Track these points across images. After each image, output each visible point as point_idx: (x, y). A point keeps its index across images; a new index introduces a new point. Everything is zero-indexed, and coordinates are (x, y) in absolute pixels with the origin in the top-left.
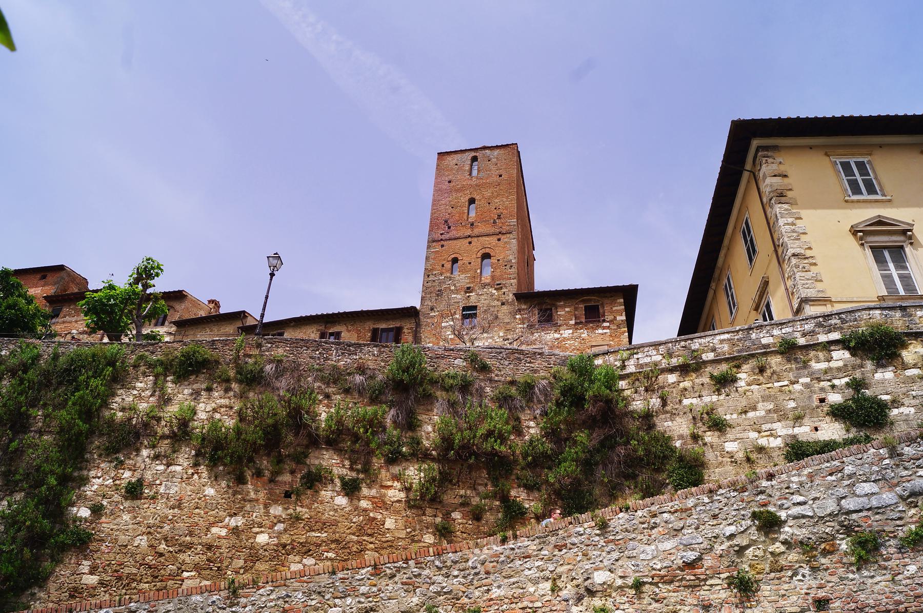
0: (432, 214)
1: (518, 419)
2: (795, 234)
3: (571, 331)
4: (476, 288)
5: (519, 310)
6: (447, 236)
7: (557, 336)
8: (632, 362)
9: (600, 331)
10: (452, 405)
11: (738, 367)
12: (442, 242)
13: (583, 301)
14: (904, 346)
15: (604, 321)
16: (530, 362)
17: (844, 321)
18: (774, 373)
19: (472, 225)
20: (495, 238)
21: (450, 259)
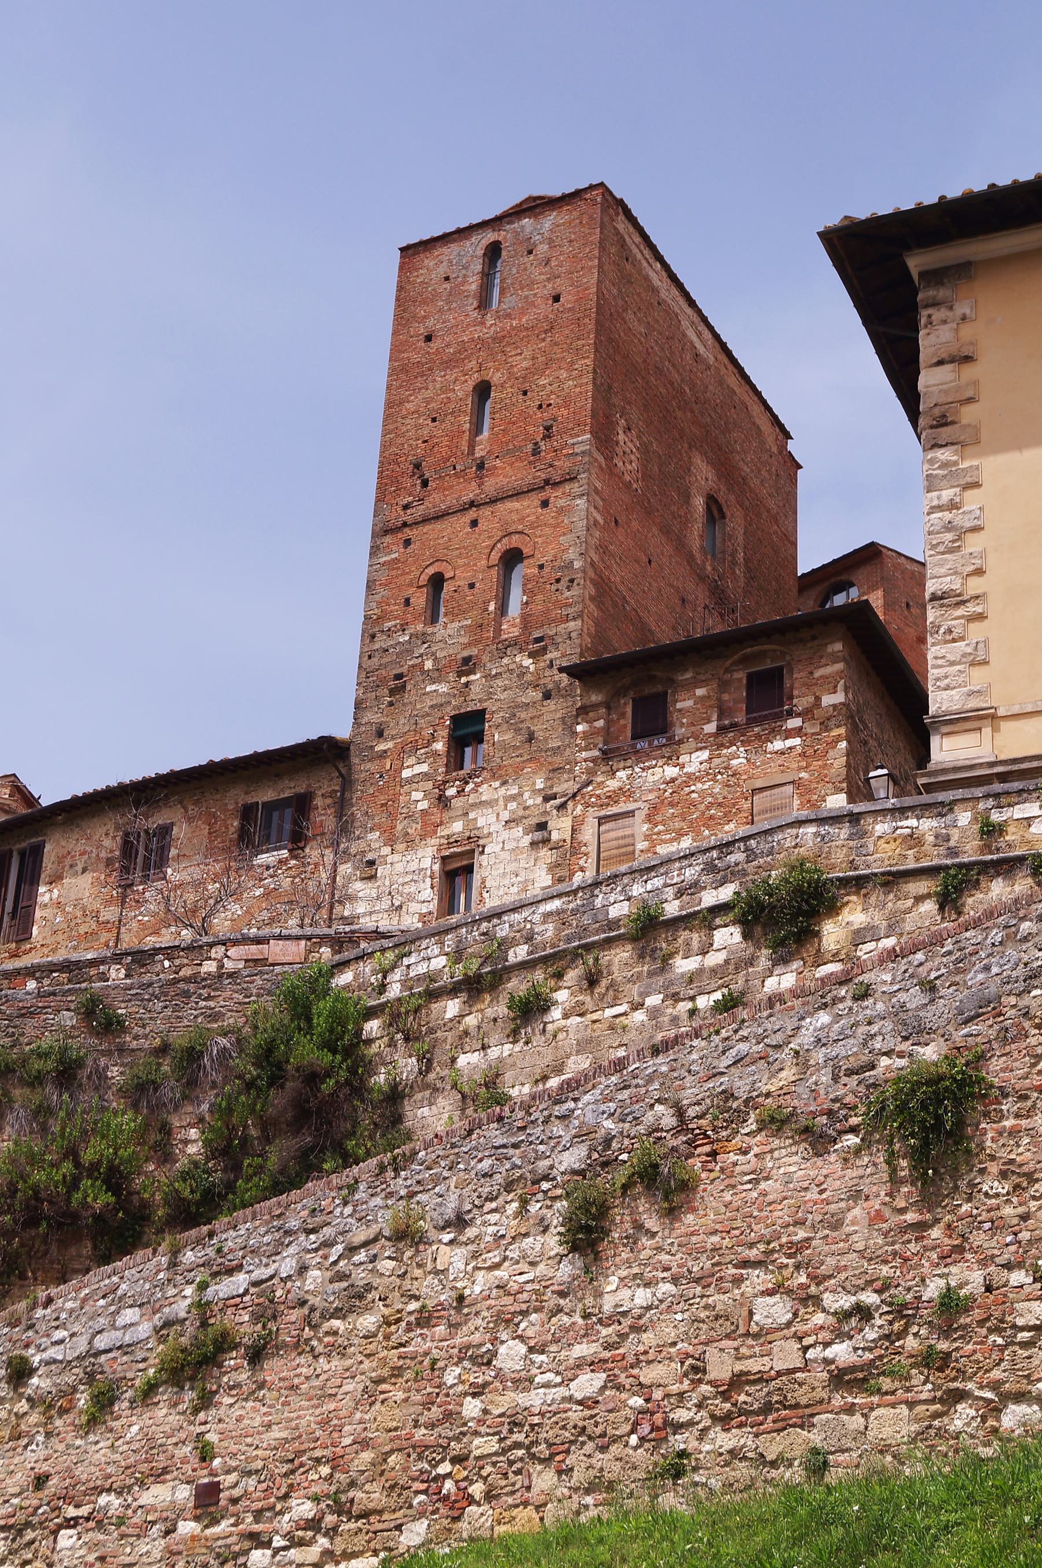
0: (384, 447)
1: (166, 1130)
2: (949, 536)
3: (705, 755)
4: (485, 658)
5: (583, 712)
6: (418, 511)
7: (671, 771)
8: (397, 975)
9: (778, 745)
10: (42, 1112)
11: (559, 976)
12: (408, 532)
13: (745, 661)
14: (833, 909)
15: (790, 714)
16: (209, 998)
17: (751, 855)
18: (612, 985)
19: (481, 466)
20: (535, 499)
21: (424, 579)
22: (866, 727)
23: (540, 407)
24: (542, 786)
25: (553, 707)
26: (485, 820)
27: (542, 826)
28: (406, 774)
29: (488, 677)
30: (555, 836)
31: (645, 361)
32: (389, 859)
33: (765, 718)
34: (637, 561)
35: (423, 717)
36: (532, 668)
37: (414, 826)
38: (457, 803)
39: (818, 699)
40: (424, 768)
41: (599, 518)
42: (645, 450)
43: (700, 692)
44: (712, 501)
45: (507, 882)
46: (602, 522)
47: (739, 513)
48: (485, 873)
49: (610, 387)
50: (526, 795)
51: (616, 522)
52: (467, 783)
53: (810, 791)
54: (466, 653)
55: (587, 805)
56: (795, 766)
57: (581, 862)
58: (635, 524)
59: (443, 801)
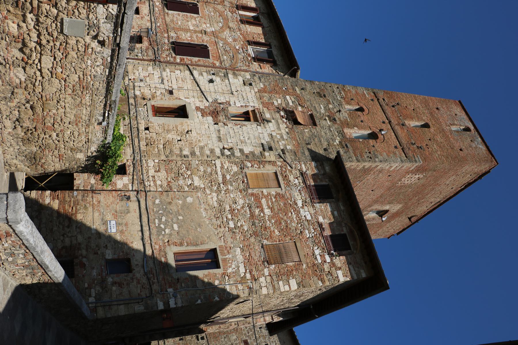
4: (336, 126)
6: (385, 107)
12: (376, 100)
15: (331, 255)
21: (362, 105)
24: (288, 148)
26: (272, 126)
27: (271, 149)
28: (288, 97)
30: (267, 154)
35: (311, 104)
36: (335, 144)
37: (267, 100)
38: (278, 115)
39: (340, 269)
40: (291, 104)
41: (393, 168)
42: (410, 186)
44: (386, 212)
45: (245, 135)
48: (249, 126)
49: (435, 171)
51: (389, 176)
52: (286, 119)
54: (337, 119)
55: (281, 167)
57: (256, 166)
59: (278, 109)
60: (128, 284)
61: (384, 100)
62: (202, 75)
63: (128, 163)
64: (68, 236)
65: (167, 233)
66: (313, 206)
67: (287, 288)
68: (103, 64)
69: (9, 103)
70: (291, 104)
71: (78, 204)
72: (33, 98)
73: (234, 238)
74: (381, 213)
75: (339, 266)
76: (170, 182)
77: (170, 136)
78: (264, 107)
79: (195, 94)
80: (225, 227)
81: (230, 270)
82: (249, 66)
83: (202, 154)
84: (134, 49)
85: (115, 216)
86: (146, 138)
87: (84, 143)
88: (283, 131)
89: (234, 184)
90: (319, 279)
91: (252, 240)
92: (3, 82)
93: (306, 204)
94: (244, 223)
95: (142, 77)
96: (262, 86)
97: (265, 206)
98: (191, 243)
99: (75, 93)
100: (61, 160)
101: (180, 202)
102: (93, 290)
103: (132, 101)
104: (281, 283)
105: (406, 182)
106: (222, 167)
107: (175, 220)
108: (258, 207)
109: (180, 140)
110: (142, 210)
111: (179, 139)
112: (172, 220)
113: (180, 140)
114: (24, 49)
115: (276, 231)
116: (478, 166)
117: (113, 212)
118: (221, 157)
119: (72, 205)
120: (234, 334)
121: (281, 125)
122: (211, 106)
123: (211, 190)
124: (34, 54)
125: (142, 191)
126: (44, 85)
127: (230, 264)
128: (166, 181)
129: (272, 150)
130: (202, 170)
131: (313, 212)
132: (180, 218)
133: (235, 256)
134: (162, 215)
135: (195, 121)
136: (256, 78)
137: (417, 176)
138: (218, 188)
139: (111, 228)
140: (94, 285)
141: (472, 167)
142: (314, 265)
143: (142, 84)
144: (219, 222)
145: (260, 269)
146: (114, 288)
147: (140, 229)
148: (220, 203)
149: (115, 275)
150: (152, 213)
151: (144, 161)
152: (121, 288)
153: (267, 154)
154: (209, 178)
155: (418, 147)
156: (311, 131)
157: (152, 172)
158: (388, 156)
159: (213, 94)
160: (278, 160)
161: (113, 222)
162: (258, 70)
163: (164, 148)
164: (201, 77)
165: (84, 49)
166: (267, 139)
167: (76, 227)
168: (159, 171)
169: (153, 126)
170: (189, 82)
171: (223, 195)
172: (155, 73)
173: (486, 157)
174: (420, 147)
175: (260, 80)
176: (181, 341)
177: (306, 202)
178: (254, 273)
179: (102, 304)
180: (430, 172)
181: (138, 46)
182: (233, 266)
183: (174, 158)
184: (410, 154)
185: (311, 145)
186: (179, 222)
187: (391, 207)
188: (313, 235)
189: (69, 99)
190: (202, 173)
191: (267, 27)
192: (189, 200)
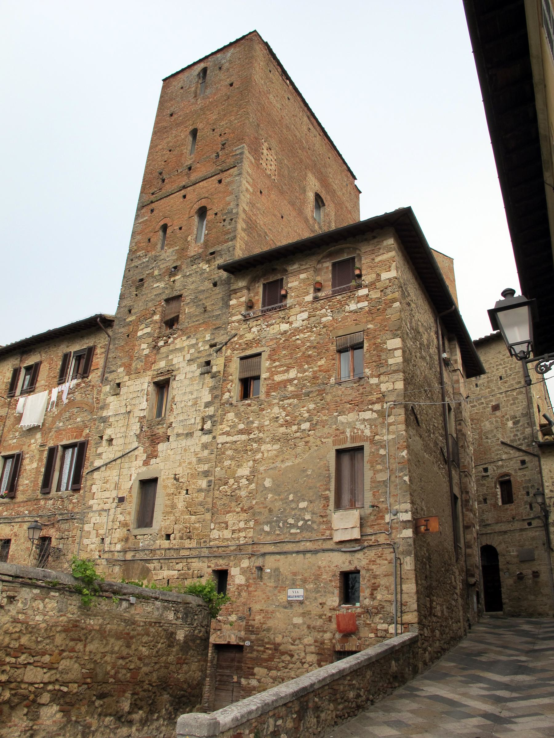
4: (184, 267)
6: (159, 195)
7: (284, 327)
12: (153, 205)
13: (330, 255)
15: (359, 287)
22: (409, 295)
23: (221, 135)
24: (209, 338)
25: (217, 291)
26: (177, 360)
27: (208, 363)
28: (140, 333)
29: (184, 276)
30: (214, 369)
31: (280, 121)
32: (128, 383)
33: (344, 290)
34: (275, 216)
35: (151, 301)
36: (208, 270)
37: (141, 364)
38: (163, 350)
39: (378, 275)
40: (148, 330)
41: (249, 187)
42: (279, 162)
43: (302, 276)
44: (318, 197)
45: (186, 398)
46: (251, 190)
47: (332, 205)
48: (175, 392)
49: (258, 125)
50: (200, 344)
51: (261, 192)
52: (169, 338)
53: (374, 338)
54: (175, 265)
55: (234, 349)
56: (365, 320)
57: (229, 386)
58: (273, 196)
59: (156, 348)
60: (375, 577)
61: (153, 194)
62: (100, 454)
63: (213, 566)
64: (305, 658)
65: (310, 518)
66: (290, 308)
67: (399, 353)
68: (43, 600)
69: (93, 729)
70: (148, 330)
71: (263, 640)
72: (87, 696)
73: (324, 424)
74: (319, 201)
75: (374, 276)
76: (242, 509)
77: (181, 506)
78: (151, 368)
79: (126, 465)
80: (309, 436)
81: (367, 432)
82: (93, 386)
83: (207, 461)
84: (58, 549)
85: (283, 589)
86: (181, 538)
87: (160, 629)
88: (186, 343)
89: (251, 419)
90: (391, 307)
91: (329, 398)
92: (59, 735)
93: (287, 318)
94: (305, 408)
95: (98, 540)
96: (122, 369)
97: (285, 377)
98: (326, 485)
99: (83, 638)
100: (186, 661)
101: (270, 496)
102: (379, 627)
103: (129, 556)
104: (391, 361)
105: (273, 167)
106: (228, 434)
107: (293, 505)
108: (285, 387)
109: (187, 490)
110: (276, 551)
111: (185, 492)
112: (293, 509)
113: (187, 490)
114: (13, 704)
115: (319, 363)
116: (256, 60)
117: (276, 592)
118: (214, 434)
119: (262, 649)
120: (482, 425)
121: (177, 347)
122: (143, 444)
123: (258, 450)
124: (20, 691)
125: (250, 550)
126: (67, 681)
127: (360, 432)
128: (240, 514)
129: (210, 361)
130: (229, 461)
131: (297, 309)
132: (291, 497)
133: (348, 423)
134: (285, 522)
135: (162, 468)
136: (111, 377)
137: (265, 151)
138: (256, 442)
139: (298, 596)
140: (373, 625)
141: (257, 69)
142: (370, 312)
143: (107, 541)
144: (302, 444)
145: (369, 389)
146: (379, 597)
147: (301, 556)
148: (275, 440)
149: (361, 594)
150: (282, 537)
151: (211, 543)
152: (379, 586)
153: (214, 369)
154: (242, 451)
155: (222, 149)
156: (188, 303)
157: (227, 534)
158: (231, 193)
159: (127, 441)
160: (223, 353)
161: (290, 592)
162: (99, 374)
163: (195, 514)
164: (104, 456)
165: (18, 625)
166: (194, 367)
167: (292, 644)
168: (226, 523)
169: (165, 528)
170: (108, 473)
171: (265, 435)
172: (93, 520)
173: (244, 48)
174: (223, 145)
175: (113, 371)
176: (488, 501)
177: (284, 318)
178: (374, 397)
179: (399, 614)
180: (261, 132)
181: (54, 543)
182: (362, 427)
183: (209, 500)
184: (230, 161)
185: (207, 304)
186: (296, 500)
187: (311, 188)
188: (329, 311)
189: (90, 647)
190: (233, 463)
191: (41, 355)
192: (268, 483)
